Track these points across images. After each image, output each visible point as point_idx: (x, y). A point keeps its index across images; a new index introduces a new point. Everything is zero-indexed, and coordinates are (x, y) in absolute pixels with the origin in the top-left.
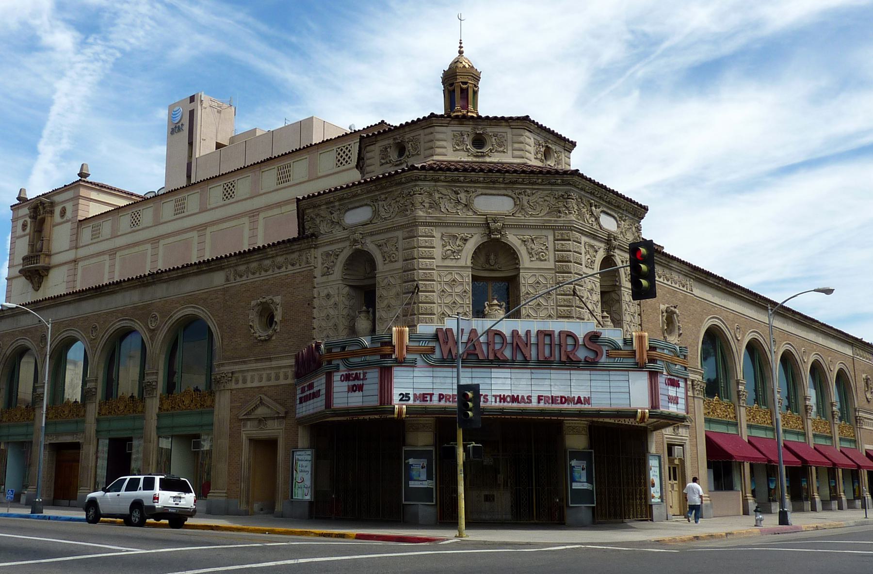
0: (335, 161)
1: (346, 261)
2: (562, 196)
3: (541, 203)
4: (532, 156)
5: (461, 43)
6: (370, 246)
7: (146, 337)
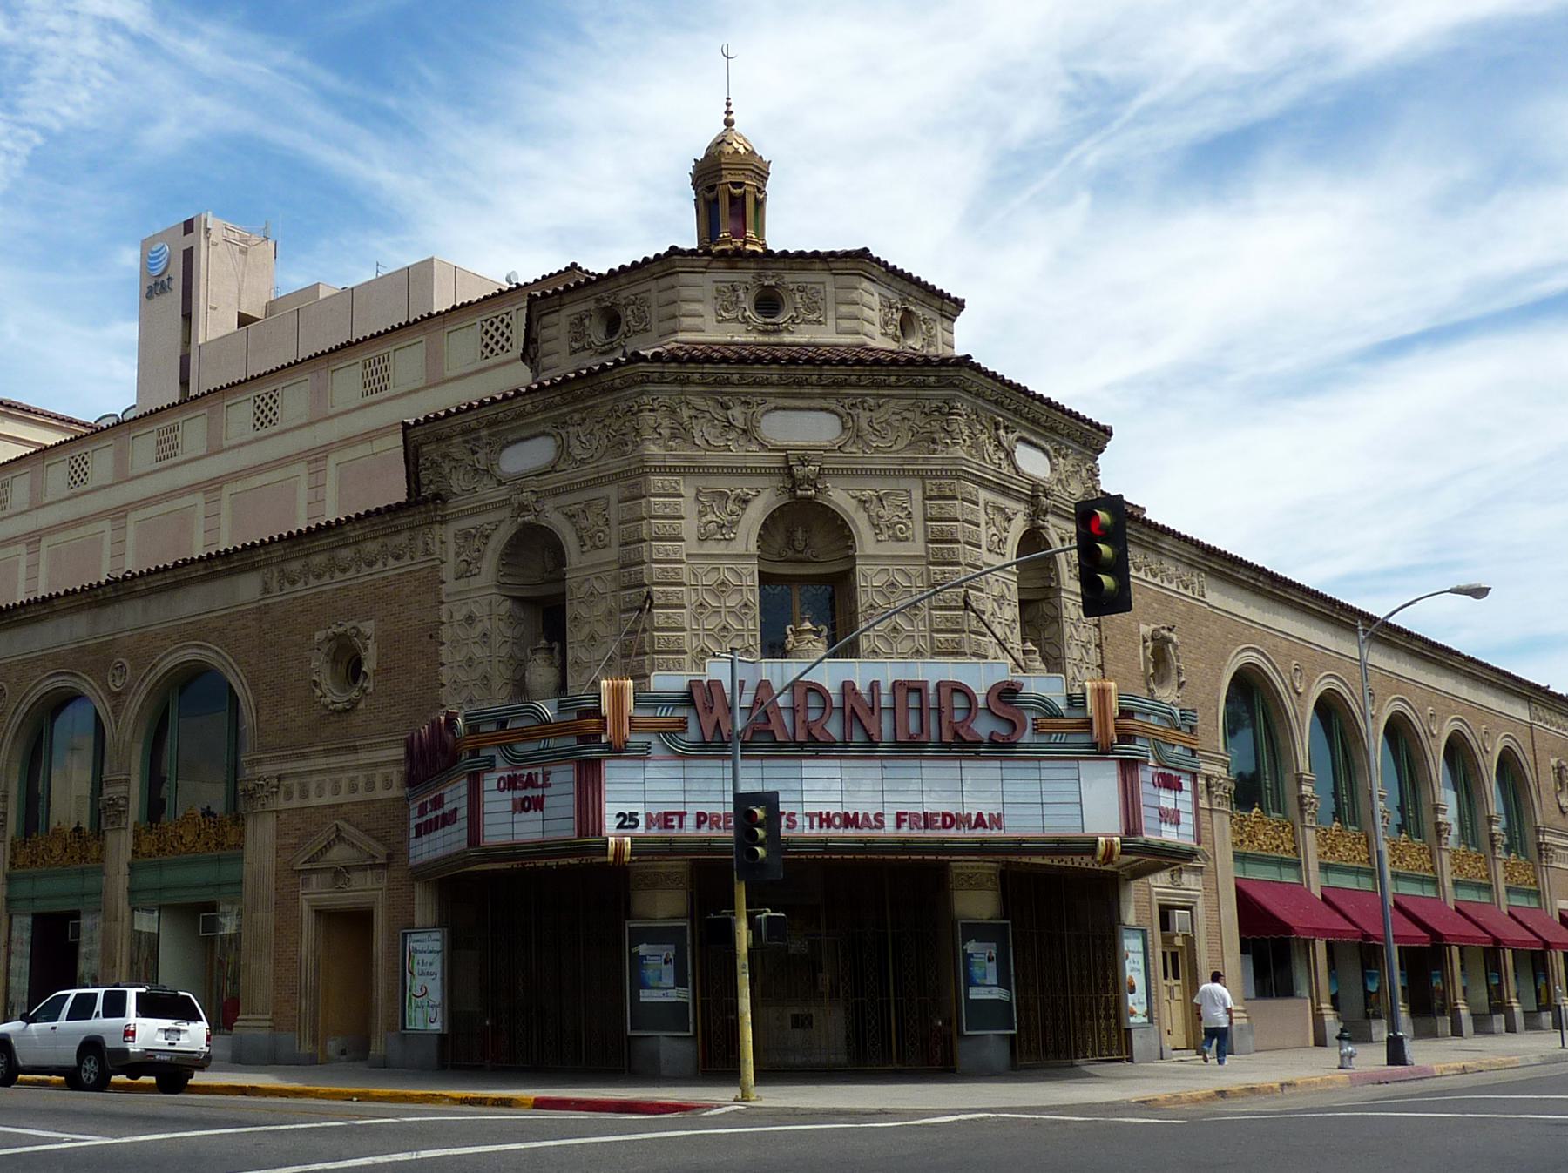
0: (480, 347)
1: (506, 547)
2: (939, 409)
3: (897, 424)
4: (876, 330)
5: (728, 105)
6: (553, 518)
7: (104, 708)
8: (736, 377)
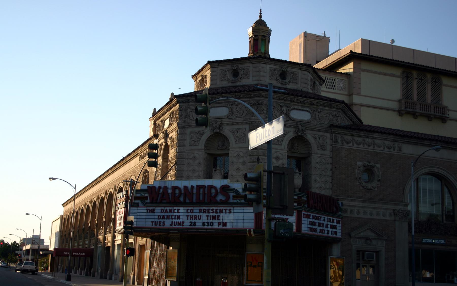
5: (261, 11)
8: (286, 98)
